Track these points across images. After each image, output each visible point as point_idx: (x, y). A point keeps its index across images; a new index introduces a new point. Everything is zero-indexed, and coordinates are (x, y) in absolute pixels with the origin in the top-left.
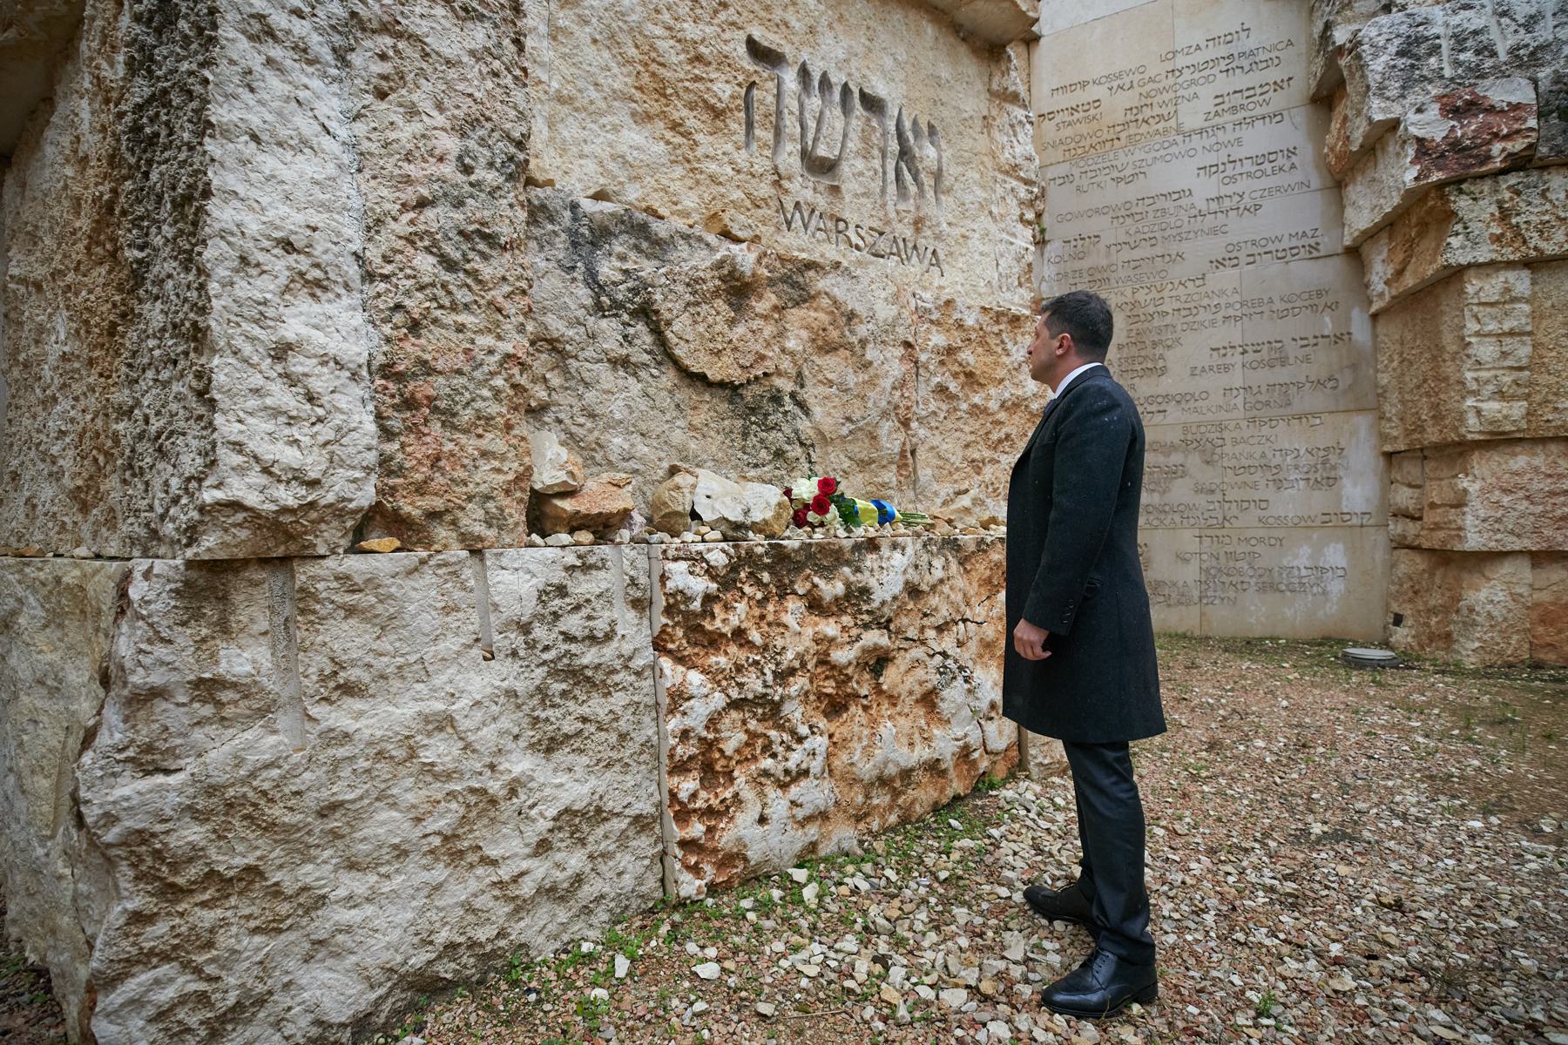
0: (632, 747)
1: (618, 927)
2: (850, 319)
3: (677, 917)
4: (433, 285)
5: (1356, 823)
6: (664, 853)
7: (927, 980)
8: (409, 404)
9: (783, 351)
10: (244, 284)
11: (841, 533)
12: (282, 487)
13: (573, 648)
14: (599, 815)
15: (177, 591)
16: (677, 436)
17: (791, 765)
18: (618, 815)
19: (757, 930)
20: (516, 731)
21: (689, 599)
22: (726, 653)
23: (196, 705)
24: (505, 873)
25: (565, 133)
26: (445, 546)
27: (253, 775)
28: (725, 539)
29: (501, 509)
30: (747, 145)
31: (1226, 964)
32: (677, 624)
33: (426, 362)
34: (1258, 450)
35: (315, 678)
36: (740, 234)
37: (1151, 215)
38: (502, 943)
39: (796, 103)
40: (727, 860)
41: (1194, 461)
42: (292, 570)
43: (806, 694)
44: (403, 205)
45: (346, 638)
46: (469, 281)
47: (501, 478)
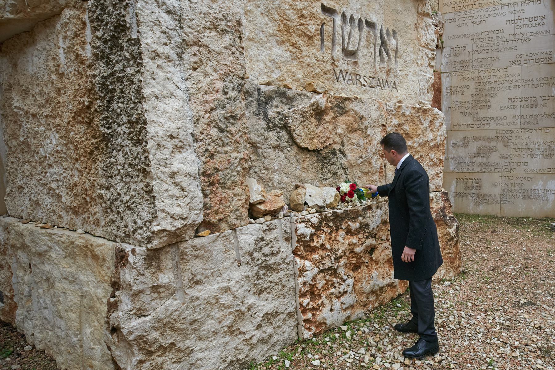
0: (287, 289)
1: (284, 350)
2: (361, 119)
3: (304, 346)
4: (217, 139)
5: (536, 298)
6: (298, 324)
7: (388, 361)
8: (212, 184)
9: (336, 134)
10: (159, 153)
11: (358, 204)
12: (176, 221)
13: (267, 258)
14: (276, 314)
15: (144, 259)
16: (298, 172)
17: (341, 290)
18: (282, 313)
19: (331, 348)
20: (249, 289)
21: (305, 237)
22: (318, 253)
23: (152, 294)
24: (247, 336)
25: (252, 53)
26: (225, 230)
27: (171, 314)
28: (317, 212)
29: (241, 213)
30: (321, 48)
31: (482, 350)
32: (301, 245)
33: (216, 168)
34: (525, 141)
35: (187, 281)
36: (320, 91)
37: (487, 39)
38: (247, 359)
39: (340, 29)
40: (320, 324)
41: (500, 145)
42: (178, 246)
43: (346, 264)
44: (205, 111)
45: (196, 266)
46: (228, 135)
47: (241, 202)
